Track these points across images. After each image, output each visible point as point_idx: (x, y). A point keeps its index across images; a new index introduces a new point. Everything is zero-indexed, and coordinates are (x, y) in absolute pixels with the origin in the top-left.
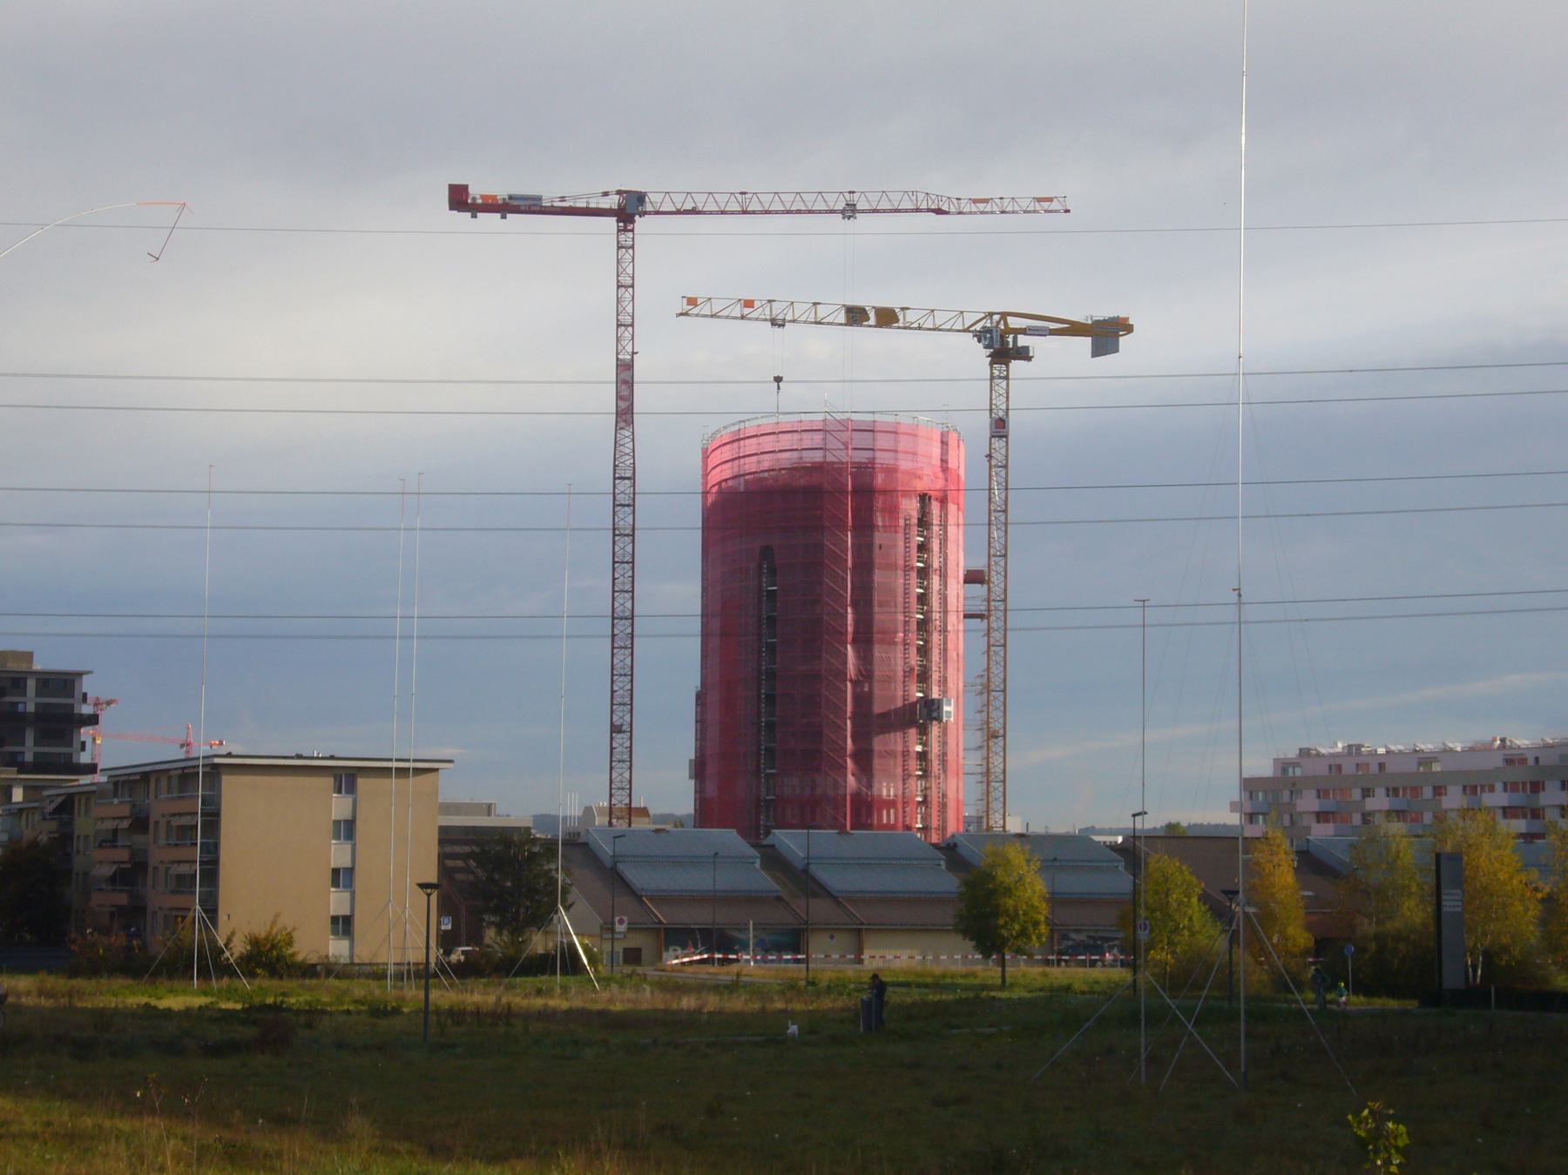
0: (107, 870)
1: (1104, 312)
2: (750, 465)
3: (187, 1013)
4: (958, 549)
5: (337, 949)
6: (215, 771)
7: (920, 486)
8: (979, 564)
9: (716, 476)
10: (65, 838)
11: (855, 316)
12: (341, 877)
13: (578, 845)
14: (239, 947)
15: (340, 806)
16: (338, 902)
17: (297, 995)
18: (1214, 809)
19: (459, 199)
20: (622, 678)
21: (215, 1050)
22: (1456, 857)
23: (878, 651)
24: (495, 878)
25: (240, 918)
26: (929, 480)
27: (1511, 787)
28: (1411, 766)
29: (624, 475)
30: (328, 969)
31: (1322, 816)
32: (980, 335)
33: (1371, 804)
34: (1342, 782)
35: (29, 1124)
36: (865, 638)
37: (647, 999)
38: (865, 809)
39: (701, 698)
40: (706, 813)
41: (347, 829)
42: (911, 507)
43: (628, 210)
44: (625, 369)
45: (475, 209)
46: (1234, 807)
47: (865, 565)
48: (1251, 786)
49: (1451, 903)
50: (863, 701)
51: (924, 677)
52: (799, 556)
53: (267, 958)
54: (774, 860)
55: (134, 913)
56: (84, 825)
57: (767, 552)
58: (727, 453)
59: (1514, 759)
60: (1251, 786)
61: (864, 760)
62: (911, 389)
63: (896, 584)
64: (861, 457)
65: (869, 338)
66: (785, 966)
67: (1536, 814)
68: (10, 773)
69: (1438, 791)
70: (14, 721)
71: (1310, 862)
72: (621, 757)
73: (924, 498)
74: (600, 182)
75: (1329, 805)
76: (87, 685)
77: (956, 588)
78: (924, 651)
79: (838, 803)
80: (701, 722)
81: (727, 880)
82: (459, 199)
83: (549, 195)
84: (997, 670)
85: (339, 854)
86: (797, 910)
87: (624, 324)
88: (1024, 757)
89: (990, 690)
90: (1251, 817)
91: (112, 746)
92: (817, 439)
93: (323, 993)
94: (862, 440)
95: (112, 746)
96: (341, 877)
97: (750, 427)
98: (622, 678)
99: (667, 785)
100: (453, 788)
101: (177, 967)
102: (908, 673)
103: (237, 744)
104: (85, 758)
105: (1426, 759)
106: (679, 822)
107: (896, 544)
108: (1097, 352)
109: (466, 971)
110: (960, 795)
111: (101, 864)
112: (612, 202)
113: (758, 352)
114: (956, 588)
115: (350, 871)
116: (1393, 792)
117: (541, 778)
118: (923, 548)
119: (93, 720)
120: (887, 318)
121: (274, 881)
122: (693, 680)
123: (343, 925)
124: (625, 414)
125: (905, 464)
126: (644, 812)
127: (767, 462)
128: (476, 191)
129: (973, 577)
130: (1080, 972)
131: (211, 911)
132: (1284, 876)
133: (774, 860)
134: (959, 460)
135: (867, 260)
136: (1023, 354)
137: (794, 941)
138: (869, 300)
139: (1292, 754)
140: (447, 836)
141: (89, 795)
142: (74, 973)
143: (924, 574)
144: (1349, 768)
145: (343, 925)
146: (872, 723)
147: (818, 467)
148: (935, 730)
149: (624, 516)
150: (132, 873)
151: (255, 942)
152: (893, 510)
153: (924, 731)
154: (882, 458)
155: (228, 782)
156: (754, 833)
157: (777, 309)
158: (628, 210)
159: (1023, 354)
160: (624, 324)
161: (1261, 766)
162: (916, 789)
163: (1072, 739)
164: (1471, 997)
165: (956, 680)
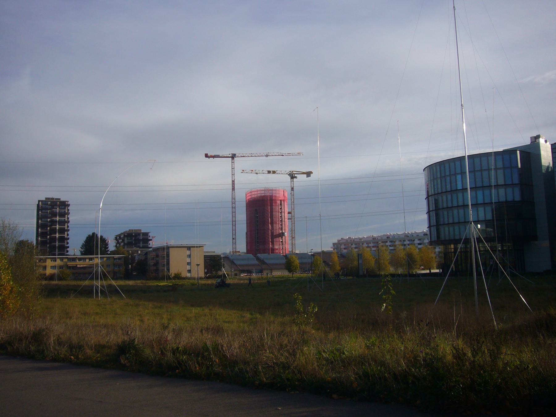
0: (152, 264)
1: (308, 170)
2: (253, 196)
3: (163, 286)
4: (287, 209)
5: (189, 275)
6: (168, 248)
7: (280, 199)
8: (290, 211)
9: (248, 198)
10: (146, 259)
11: (269, 172)
12: (189, 264)
13: (226, 258)
14: (173, 275)
15: (188, 252)
16: (188, 268)
17: (181, 282)
18: (328, 248)
19: (207, 156)
20: (234, 231)
21: (165, 291)
22: (361, 254)
23: (274, 225)
24: (213, 263)
25: (173, 270)
26: (282, 198)
27: (374, 243)
28: (358, 240)
29: (233, 198)
30: (189, 279)
31: (345, 249)
32: (289, 175)
33: (352, 246)
34: (348, 243)
35: (132, 303)
36: (272, 223)
37: (236, 281)
38: (273, 250)
39: (246, 233)
40: (248, 251)
41: (189, 256)
42: (279, 202)
43: (233, 157)
44: (233, 182)
45: (209, 157)
46: (331, 248)
47: (272, 211)
48: (334, 244)
49: (360, 262)
50: (272, 233)
51: (282, 229)
52: (261, 211)
53: (177, 277)
54: (258, 259)
55: (157, 270)
56: (149, 257)
57: (256, 210)
58: (249, 194)
59: (374, 238)
60: (334, 244)
61: (273, 243)
62: (278, 183)
63: (277, 214)
64: (271, 194)
65: (271, 175)
66: (259, 275)
67: (395, 246)
68: (138, 249)
69: (363, 244)
70: (139, 240)
71: (342, 256)
72: (234, 243)
73: (281, 200)
74: (228, 153)
75: (346, 247)
76: (150, 234)
77: (286, 215)
78: (282, 225)
79: (269, 249)
80: (247, 237)
81: (251, 262)
82: (207, 156)
83: (221, 155)
84: (293, 227)
85: (188, 260)
86: (262, 266)
87: (233, 175)
88: (298, 241)
89: (292, 231)
90: (334, 249)
91: (154, 244)
92: (263, 192)
93: (185, 282)
94: (270, 192)
95: (154, 244)
96: (189, 264)
97: (253, 190)
98: (234, 231)
99: (242, 247)
100: (206, 249)
101: (163, 279)
102: (279, 228)
103: (172, 243)
104: (150, 246)
105: (361, 239)
106: (420, 237)
107: (277, 208)
108: (307, 177)
109: (208, 278)
110: (288, 248)
111: (151, 262)
112: (231, 155)
113: (253, 178)
114: (286, 215)
115: (190, 263)
116: (355, 244)
117: (221, 247)
118: (281, 209)
119: (151, 240)
120: (274, 172)
121: (178, 265)
122: (246, 231)
123: (189, 271)
124: (233, 189)
125: (277, 195)
126: (239, 252)
127: (256, 196)
128: (209, 155)
129: (289, 213)
130: (306, 275)
131: (168, 270)
132: (336, 258)
133: (258, 259)
134: (286, 194)
135: (272, 163)
136: (296, 177)
137: (261, 271)
138: (271, 170)
139: (340, 239)
140: (205, 257)
141: (150, 252)
142: (147, 280)
143: (281, 213)
144: (349, 241)
145: (189, 271)
146: (274, 237)
147: (264, 196)
148: (284, 237)
149: (234, 205)
150: (156, 264)
151: (175, 274)
152: (276, 203)
153: (282, 238)
154: (274, 194)
155: (170, 249)
156: (255, 255)
157: (257, 172)
158: (233, 157)
159: (296, 177)
160: (233, 175)
161: (336, 241)
162: (281, 247)
163: (306, 238)
164: (364, 276)
165: (287, 229)
